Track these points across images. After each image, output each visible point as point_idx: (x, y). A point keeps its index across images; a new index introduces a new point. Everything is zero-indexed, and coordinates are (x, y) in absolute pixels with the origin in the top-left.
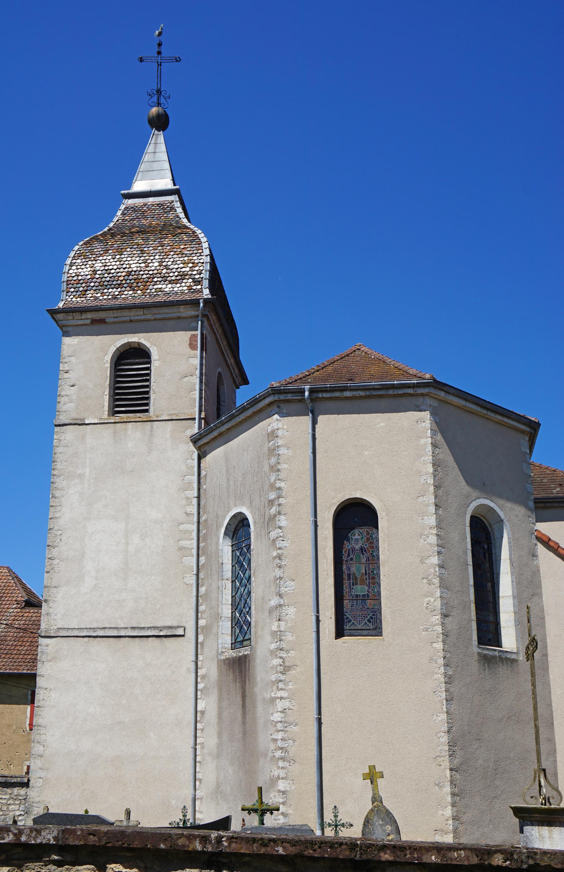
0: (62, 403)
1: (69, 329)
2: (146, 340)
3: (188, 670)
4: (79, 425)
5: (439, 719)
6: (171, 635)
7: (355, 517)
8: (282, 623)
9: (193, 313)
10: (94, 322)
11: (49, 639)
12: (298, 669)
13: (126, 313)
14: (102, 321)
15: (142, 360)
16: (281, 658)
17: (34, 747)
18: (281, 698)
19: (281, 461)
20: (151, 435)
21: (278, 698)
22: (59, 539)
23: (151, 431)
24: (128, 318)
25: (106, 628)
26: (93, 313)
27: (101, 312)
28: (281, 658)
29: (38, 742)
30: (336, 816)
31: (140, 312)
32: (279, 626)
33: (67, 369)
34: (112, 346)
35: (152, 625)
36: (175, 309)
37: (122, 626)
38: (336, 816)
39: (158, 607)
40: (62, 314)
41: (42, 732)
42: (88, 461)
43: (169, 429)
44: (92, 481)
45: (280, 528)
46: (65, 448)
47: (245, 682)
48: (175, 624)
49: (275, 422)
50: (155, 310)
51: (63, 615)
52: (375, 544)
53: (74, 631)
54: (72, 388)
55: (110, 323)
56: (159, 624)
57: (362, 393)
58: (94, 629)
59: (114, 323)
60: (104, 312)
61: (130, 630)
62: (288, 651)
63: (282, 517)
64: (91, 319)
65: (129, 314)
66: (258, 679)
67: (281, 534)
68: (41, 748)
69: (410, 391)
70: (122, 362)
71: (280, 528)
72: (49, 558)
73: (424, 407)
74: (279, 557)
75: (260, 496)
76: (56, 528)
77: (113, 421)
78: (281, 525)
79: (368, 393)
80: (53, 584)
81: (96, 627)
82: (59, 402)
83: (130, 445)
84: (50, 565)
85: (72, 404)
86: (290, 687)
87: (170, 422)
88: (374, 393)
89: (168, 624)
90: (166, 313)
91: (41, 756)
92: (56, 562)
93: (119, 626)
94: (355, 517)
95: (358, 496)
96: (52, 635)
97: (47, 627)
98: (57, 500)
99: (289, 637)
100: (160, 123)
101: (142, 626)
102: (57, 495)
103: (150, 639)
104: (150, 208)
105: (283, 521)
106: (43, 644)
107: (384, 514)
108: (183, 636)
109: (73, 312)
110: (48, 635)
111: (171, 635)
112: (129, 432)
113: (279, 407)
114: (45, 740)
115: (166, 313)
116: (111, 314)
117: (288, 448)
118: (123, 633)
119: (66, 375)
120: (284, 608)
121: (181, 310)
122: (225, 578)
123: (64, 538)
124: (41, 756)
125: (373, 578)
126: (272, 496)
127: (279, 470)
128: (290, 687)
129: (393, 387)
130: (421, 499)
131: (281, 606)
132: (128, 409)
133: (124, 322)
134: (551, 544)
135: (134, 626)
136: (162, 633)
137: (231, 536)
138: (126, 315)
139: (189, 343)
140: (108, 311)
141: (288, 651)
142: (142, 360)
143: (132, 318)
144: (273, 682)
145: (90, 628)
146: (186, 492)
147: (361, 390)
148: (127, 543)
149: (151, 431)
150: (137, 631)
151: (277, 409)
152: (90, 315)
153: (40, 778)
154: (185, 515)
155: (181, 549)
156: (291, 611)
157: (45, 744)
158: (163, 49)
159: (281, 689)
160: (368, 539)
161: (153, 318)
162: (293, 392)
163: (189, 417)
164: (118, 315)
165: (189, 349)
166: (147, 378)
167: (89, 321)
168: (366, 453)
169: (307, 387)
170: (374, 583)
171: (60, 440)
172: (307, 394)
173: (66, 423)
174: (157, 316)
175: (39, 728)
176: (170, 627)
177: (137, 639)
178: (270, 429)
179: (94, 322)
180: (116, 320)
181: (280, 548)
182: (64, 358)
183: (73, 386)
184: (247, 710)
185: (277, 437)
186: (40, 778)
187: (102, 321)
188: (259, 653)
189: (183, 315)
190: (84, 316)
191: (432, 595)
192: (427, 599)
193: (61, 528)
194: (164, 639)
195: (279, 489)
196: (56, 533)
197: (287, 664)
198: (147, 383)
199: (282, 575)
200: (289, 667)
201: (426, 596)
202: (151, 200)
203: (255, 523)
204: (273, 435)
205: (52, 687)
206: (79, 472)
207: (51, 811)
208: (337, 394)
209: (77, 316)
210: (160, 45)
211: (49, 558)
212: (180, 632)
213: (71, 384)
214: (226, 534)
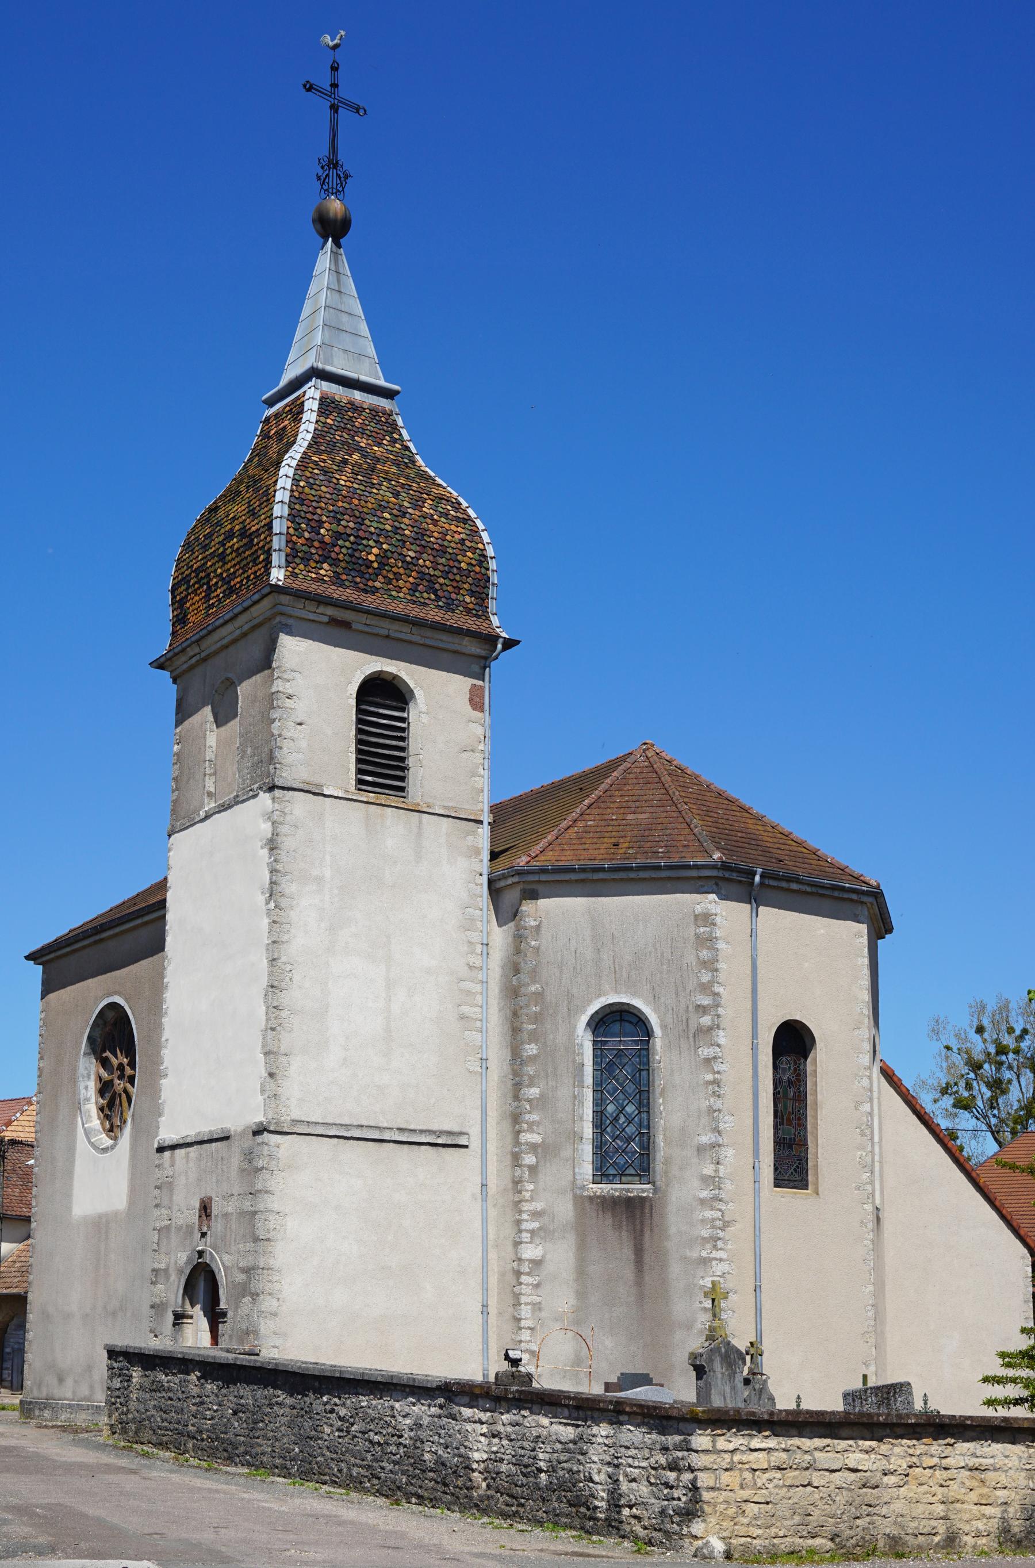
3: (473, 1196)
4: (314, 794)
5: (867, 1290)
6: (450, 1143)
7: (793, 1042)
8: (720, 1167)
9: (478, 650)
10: (334, 622)
11: (279, 1137)
12: (738, 1226)
13: (386, 624)
14: (346, 625)
15: (395, 704)
16: (720, 1210)
17: (264, 1300)
18: (721, 1260)
19: (720, 958)
20: (419, 835)
21: (715, 1259)
22: (287, 979)
23: (420, 828)
25: (362, 1126)
27: (349, 612)
28: (720, 1210)
29: (270, 1294)
30: (926, 1404)
31: (406, 628)
32: (717, 1171)
33: (290, 691)
35: (425, 1128)
37: (385, 1125)
38: (926, 1404)
39: (433, 1101)
40: (288, 597)
41: (275, 1279)
42: (328, 857)
43: (444, 830)
44: (336, 891)
45: (719, 1046)
46: (292, 829)
47: (642, 1231)
48: (456, 1129)
49: (709, 902)
50: (429, 633)
51: (298, 1100)
52: (802, 1077)
53: (318, 1127)
54: (299, 727)
56: (435, 1127)
57: (809, 889)
58: (346, 1125)
60: (354, 613)
61: (397, 1132)
62: (727, 1203)
63: (721, 1033)
66: (673, 1230)
67: (720, 1054)
68: (275, 1303)
69: (854, 897)
70: (367, 698)
71: (719, 1046)
72: (275, 1007)
73: (862, 918)
74: (716, 1083)
75: (677, 994)
76: (283, 959)
77: (365, 799)
78: (720, 1042)
79: (814, 890)
80: (283, 1049)
81: (348, 1123)
82: (281, 748)
83: (390, 843)
84: (276, 1018)
85: (300, 756)
86: (729, 1247)
87: (445, 819)
88: (821, 891)
89: (446, 1127)
91: (275, 1315)
92: (284, 1014)
93: (380, 1125)
94: (793, 1042)
95: (798, 1018)
96: (285, 1130)
97: (275, 1116)
98: (282, 913)
99: (728, 1186)
100: (334, 229)
101: (412, 1127)
102: (283, 905)
103: (423, 1147)
104: (355, 407)
105: (722, 1037)
106: (271, 1143)
107: (822, 1044)
108: (466, 1147)
109: (307, 599)
110: (279, 1129)
111: (450, 1143)
112: (388, 823)
113: (717, 884)
114: (280, 1291)
116: (363, 618)
117: (727, 943)
118: (387, 1136)
119: (289, 703)
120: (723, 1149)
122: (586, 1085)
123: (296, 978)
124: (275, 1315)
125: (799, 1119)
126: (706, 1001)
127: (717, 970)
128: (729, 1247)
129: (843, 889)
130: (856, 1032)
131: (719, 1145)
132: (377, 780)
133: (377, 635)
134: (895, 1079)
135: (401, 1126)
136: (440, 1141)
137: (593, 1027)
141: (727, 1203)
142: (395, 704)
143: (392, 634)
144: (704, 1238)
145: (341, 1125)
146: (468, 933)
147: (808, 885)
148: (389, 1000)
149: (420, 828)
150: (406, 1134)
151: (714, 887)
152: (330, 611)
153: (274, 1347)
154: (466, 968)
155: (462, 1017)
156: (728, 1153)
157: (280, 1296)
159: (721, 1249)
160: (795, 1070)
161: (421, 642)
162: (740, 871)
163: (473, 818)
164: (373, 623)
167: (326, 619)
168: (806, 965)
169: (759, 870)
170: (800, 1125)
171: (285, 814)
172: (757, 878)
173: (295, 786)
174: (429, 642)
175: (270, 1272)
176: (450, 1133)
177: (406, 1146)
178: (699, 909)
179: (334, 622)
180: (367, 629)
181: (718, 1073)
182: (285, 671)
183: (300, 724)
184: (646, 1267)
185: (715, 925)
186: (274, 1347)
187: (346, 625)
188: (674, 1199)
191: (863, 1149)
192: (859, 1153)
193: (292, 961)
194: (441, 1149)
195: (718, 994)
196: (283, 966)
197: (727, 1219)
199: (721, 1107)
200: (728, 1222)
201: (858, 1149)
202: (358, 396)
203: (664, 1027)
204: (706, 919)
205: (287, 1211)
206: (316, 872)
207: (804, 1406)
208: (784, 884)
209: (311, 606)
210: (335, 69)
211: (275, 1007)
212: (463, 1141)
213: (299, 720)
214: (588, 1024)
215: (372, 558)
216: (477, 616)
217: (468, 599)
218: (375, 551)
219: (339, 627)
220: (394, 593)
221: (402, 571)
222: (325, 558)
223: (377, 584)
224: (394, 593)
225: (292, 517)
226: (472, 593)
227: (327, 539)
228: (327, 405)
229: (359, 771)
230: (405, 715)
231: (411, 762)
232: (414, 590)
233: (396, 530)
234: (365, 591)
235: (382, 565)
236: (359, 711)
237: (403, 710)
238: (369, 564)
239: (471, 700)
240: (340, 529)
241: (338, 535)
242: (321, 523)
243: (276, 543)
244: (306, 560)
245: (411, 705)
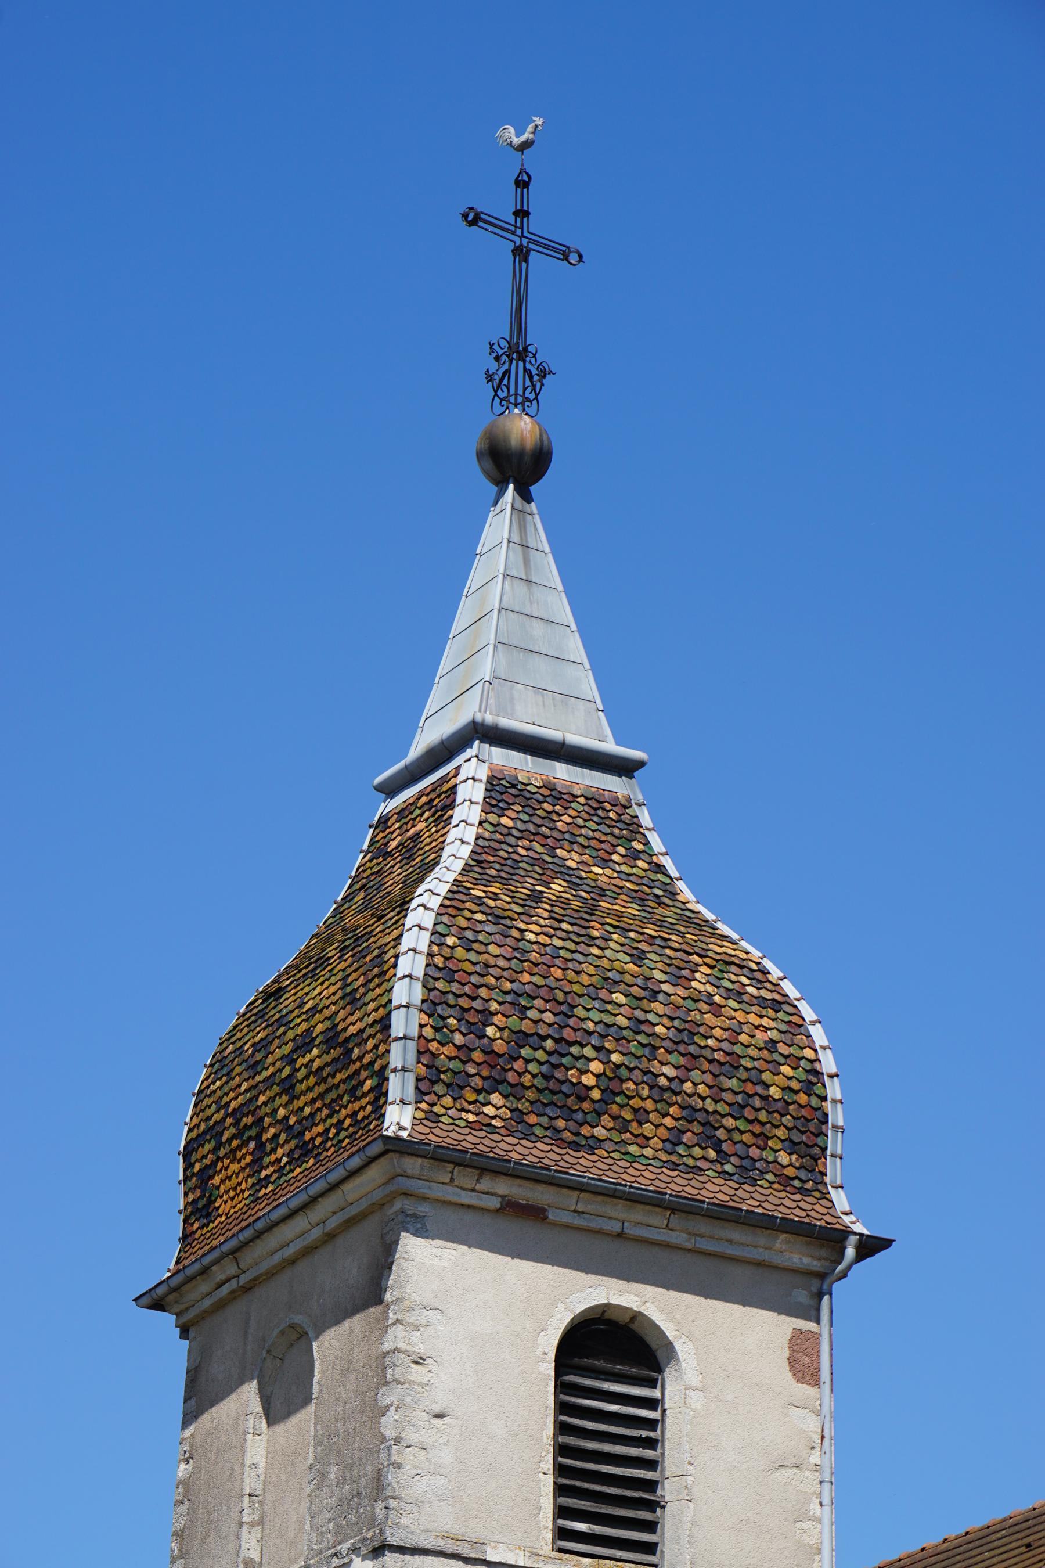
0: (408, 1470)
1: (423, 1209)
2: (662, 1312)
4: (466, 1560)
9: (806, 1260)
10: (511, 1208)
13: (618, 1210)
14: (535, 1213)
15: (634, 1371)
24: (617, 1227)
26: (518, 1181)
27: (541, 1188)
31: (658, 1218)
34: (561, 1306)
36: (761, 1238)
50: (704, 1226)
54: (437, 1422)
55: (555, 1224)
59: (567, 1227)
60: (552, 1190)
64: (503, 1197)
65: (622, 1216)
70: (576, 1361)
82: (399, 1466)
85: (440, 1482)
90: (730, 1241)
100: (518, 469)
115: (730, 1241)
116: (571, 1199)
119: (417, 1373)
121: (778, 1246)
132: (598, 1529)
138: (613, 1214)
139: (787, 1355)
140: (564, 1191)
142: (634, 1371)
143: (630, 1230)
152: (504, 1187)
158: (536, 199)
164: (590, 1208)
165: (789, 1375)
166: (651, 1434)
167: (494, 1203)
173: (427, 1545)
174: (704, 1245)
179: (511, 1208)
180: (578, 1221)
182: (410, 1309)
183: (440, 1416)
187: (535, 1213)
189: (777, 1260)
190: (485, 1184)
198: (648, 1453)
202: (562, 772)
209: (466, 1178)
213: (437, 1409)
215: (588, 1080)
216: (804, 1192)
217: (784, 1158)
218: (596, 1067)
219: (523, 1218)
220: (633, 1149)
221: (649, 1105)
222: (495, 1084)
223: (599, 1132)
224: (633, 1149)
225: (431, 1006)
226: (792, 1147)
227: (499, 1046)
228: (501, 791)
229: (561, 1512)
230: (656, 1394)
231: (668, 1491)
232: (673, 1141)
233: (638, 1025)
234: (576, 1146)
235: (610, 1094)
236: (561, 1387)
237: (652, 1383)
238: (582, 1093)
239: (792, 1361)
240: (526, 1026)
241: (521, 1038)
242: (486, 1016)
243: (398, 1055)
244: (456, 1088)
245: (669, 1374)
